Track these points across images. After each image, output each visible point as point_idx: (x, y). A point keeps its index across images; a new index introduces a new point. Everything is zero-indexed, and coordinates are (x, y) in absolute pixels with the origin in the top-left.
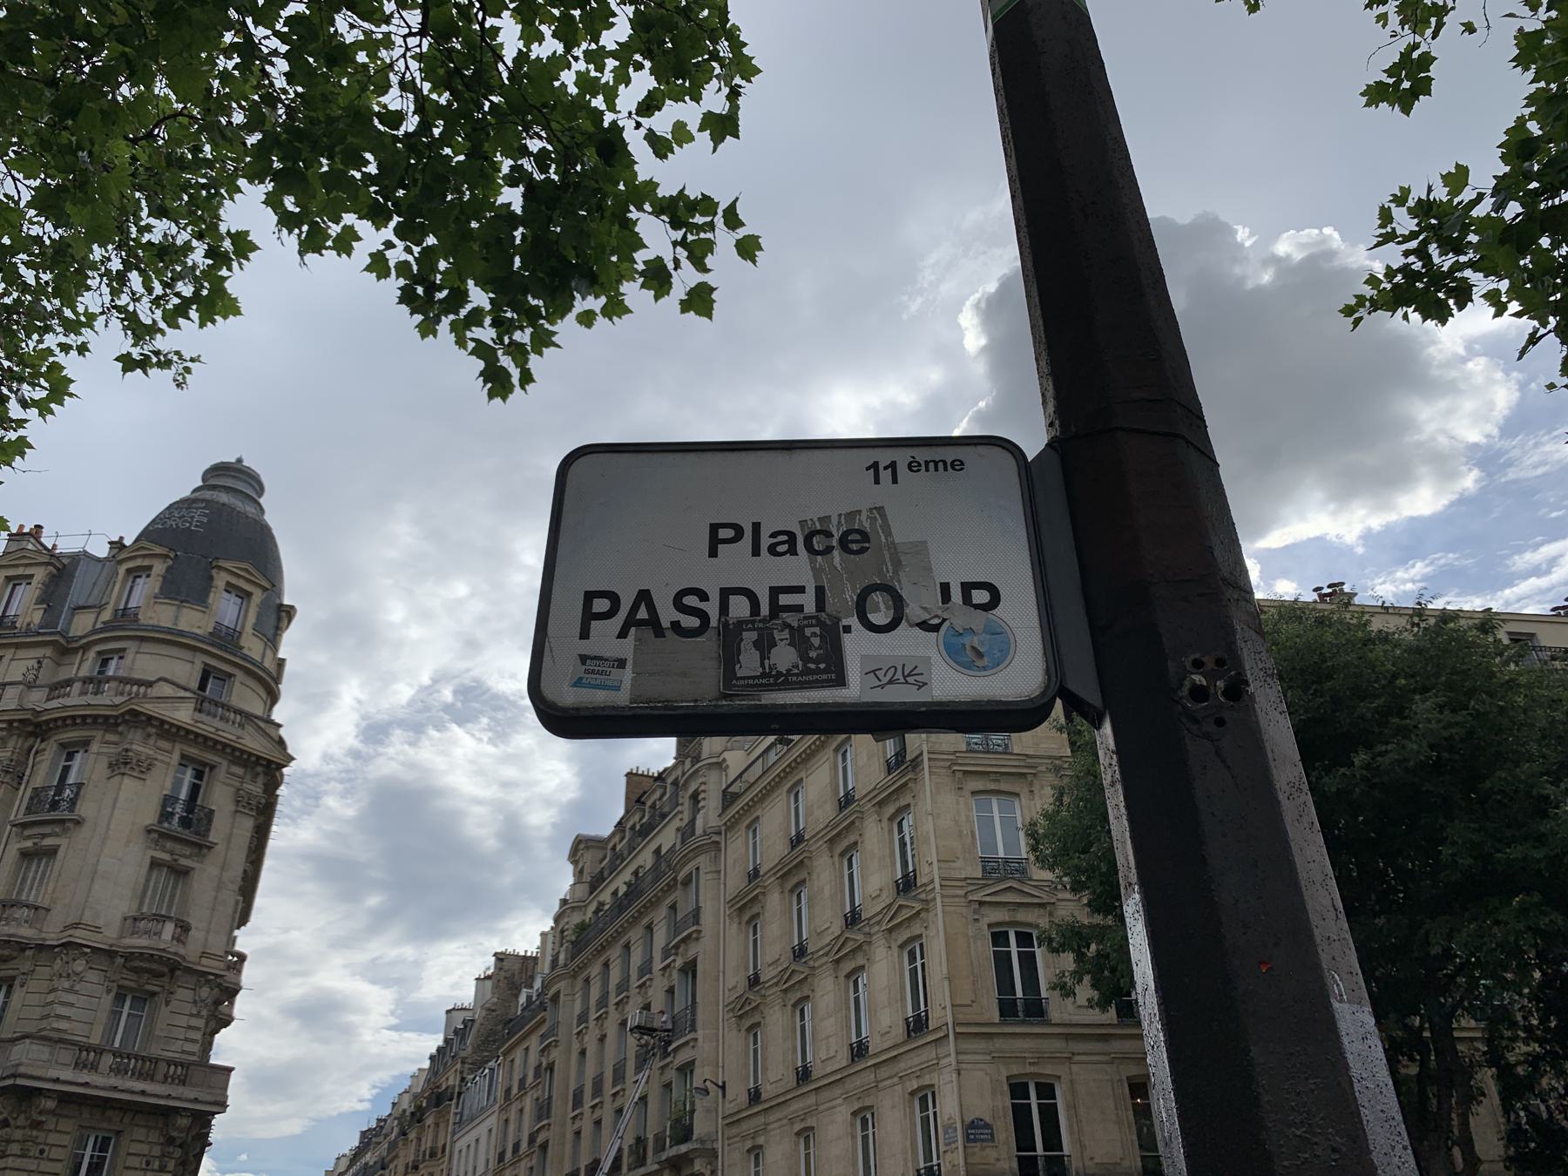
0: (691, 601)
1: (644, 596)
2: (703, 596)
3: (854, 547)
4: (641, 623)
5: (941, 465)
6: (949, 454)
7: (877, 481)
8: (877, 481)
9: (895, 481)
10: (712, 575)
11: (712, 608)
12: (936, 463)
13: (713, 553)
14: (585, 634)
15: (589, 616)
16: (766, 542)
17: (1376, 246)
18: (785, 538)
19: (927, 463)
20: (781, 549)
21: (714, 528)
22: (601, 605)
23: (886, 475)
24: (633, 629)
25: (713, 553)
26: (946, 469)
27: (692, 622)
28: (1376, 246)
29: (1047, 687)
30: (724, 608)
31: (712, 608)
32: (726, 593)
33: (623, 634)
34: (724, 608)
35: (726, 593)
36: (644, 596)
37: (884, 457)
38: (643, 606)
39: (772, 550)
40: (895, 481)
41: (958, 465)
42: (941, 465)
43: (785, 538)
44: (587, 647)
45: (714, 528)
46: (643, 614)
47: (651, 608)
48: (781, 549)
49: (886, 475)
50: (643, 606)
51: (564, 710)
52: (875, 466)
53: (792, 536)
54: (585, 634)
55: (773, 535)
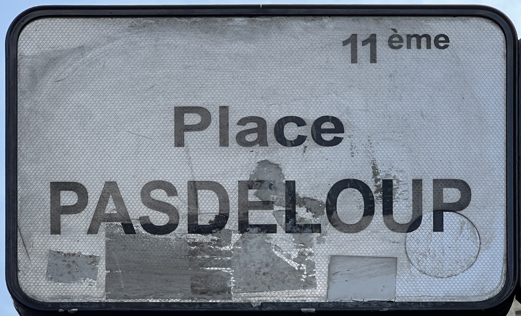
0: (159, 195)
1: (111, 189)
2: (171, 191)
3: (442, 45)
4: (110, 218)
5: (424, 40)
6: (436, 26)
7: (354, 60)
8: (354, 60)
9: (373, 59)
10: (177, 168)
11: (180, 203)
12: (419, 38)
13: (179, 142)
14: (56, 229)
15: (58, 211)
16: (234, 130)
17: (374, 168)
18: (253, 125)
19: (409, 37)
20: (250, 138)
21: (180, 112)
22: (68, 198)
23: (363, 51)
24: (103, 225)
25: (179, 142)
26: (429, 47)
27: (160, 219)
28: (374, 168)
29: (504, 290)
30: (193, 201)
31: (180, 203)
32: (194, 187)
33: (92, 230)
34: (193, 201)
35: (194, 187)
36: (111, 189)
37: (364, 27)
38: (111, 200)
39: (241, 139)
40: (373, 59)
41: (442, 42)
42: (424, 40)
43: (253, 125)
44: (62, 244)
45: (180, 112)
46: (111, 207)
47: (119, 201)
48: (250, 138)
49: (363, 51)
50: (111, 200)
51: (44, 304)
52: (352, 40)
53: (261, 122)
54: (56, 229)
55: (242, 122)
